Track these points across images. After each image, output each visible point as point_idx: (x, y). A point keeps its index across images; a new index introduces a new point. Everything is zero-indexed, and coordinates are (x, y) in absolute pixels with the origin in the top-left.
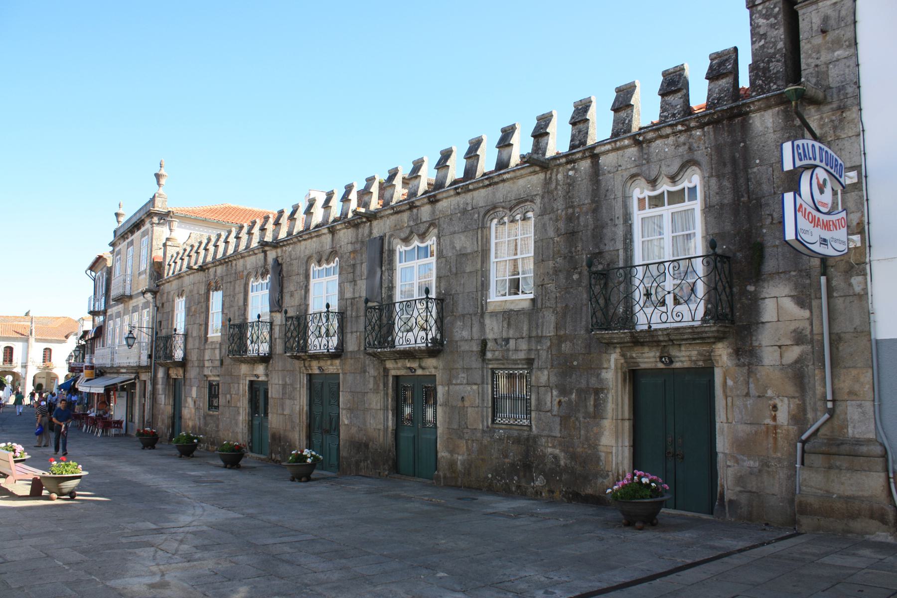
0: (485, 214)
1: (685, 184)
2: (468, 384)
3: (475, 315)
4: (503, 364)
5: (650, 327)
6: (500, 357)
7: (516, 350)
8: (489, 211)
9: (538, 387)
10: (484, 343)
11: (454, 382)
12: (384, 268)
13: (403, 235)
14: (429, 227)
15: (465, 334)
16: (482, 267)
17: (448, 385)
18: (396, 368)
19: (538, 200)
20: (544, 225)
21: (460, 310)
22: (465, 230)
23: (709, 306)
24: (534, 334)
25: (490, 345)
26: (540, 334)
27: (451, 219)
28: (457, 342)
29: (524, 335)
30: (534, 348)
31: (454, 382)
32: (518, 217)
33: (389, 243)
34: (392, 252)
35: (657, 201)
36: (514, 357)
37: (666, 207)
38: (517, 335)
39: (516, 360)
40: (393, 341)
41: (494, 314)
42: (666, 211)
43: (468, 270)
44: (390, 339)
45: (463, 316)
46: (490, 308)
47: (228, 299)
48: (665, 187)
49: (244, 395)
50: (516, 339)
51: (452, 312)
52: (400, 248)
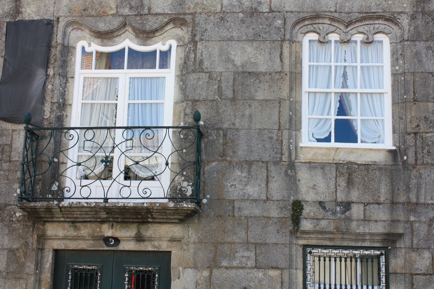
0: (297, 23)
1: (158, 46)
2: (257, 267)
3: (276, 163)
4: (331, 239)
5: (34, 224)
6: (331, 228)
7: (366, 220)
8: (304, 19)
9: (412, 275)
10: (297, 207)
11: (225, 263)
12: (51, 72)
13: (102, 27)
14: (167, 24)
15: (253, 190)
16: (290, 96)
17: (210, 268)
18: (59, 236)
19: (405, 21)
20: (417, 54)
21: (242, 153)
22: (255, 38)
23: (158, 205)
24: (402, 198)
25: (307, 210)
26: (414, 200)
27: (222, 19)
28: (233, 201)
29: (382, 199)
30: (402, 218)
31: (225, 263)
32: (359, 38)
33: (65, 34)
34: (67, 50)
35: (112, 61)
36: (361, 230)
37: (125, 70)
38: (368, 198)
39: (364, 234)
40: (61, 189)
41: (312, 165)
42: (124, 75)
43: (260, 96)
44: (55, 188)
45: (250, 163)
46: (303, 157)
47: (138, 67)
48: (127, 42)
49: (154, 246)
50: (366, 205)
51: (223, 155)
52: (85, 44)
